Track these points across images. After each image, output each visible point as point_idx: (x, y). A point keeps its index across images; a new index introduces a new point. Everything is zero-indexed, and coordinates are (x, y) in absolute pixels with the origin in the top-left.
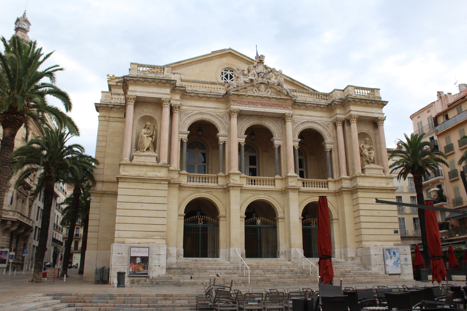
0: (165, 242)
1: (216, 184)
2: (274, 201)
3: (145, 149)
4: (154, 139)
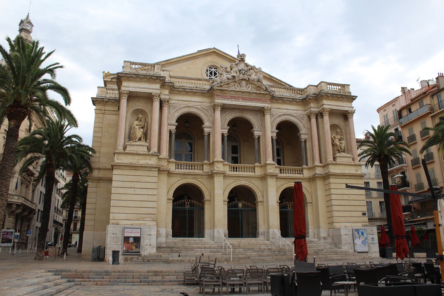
0: (155, 224)
1: (201, 171)
2: (254, 186)
3: (137, 139)
4: (145, 130)
